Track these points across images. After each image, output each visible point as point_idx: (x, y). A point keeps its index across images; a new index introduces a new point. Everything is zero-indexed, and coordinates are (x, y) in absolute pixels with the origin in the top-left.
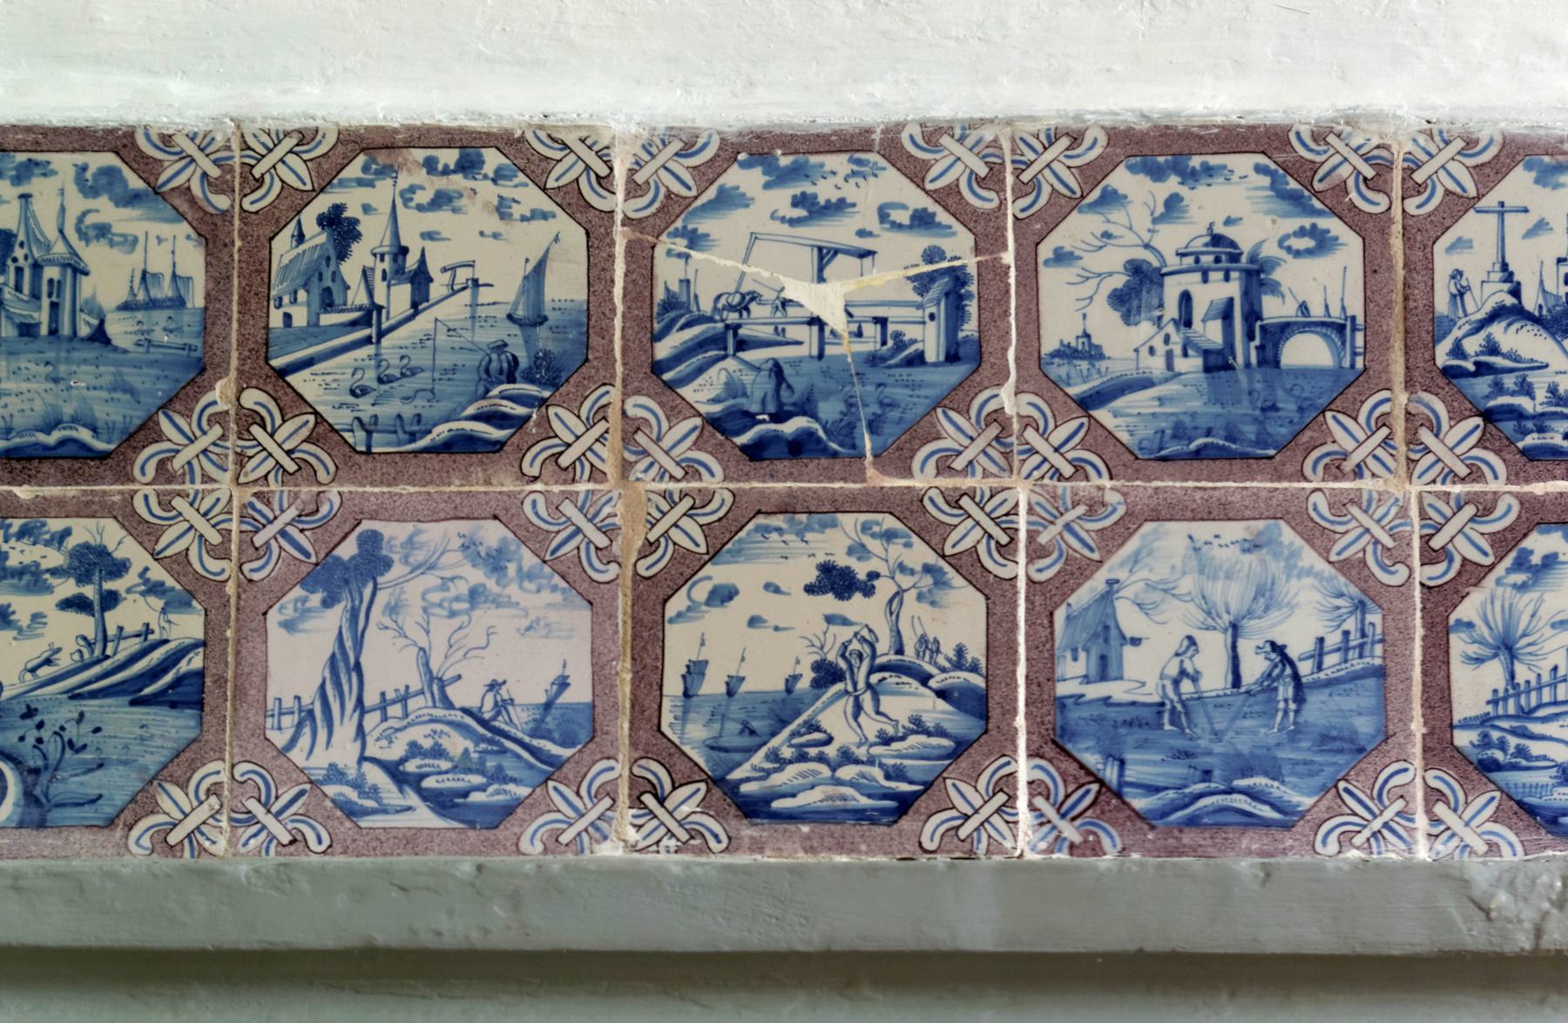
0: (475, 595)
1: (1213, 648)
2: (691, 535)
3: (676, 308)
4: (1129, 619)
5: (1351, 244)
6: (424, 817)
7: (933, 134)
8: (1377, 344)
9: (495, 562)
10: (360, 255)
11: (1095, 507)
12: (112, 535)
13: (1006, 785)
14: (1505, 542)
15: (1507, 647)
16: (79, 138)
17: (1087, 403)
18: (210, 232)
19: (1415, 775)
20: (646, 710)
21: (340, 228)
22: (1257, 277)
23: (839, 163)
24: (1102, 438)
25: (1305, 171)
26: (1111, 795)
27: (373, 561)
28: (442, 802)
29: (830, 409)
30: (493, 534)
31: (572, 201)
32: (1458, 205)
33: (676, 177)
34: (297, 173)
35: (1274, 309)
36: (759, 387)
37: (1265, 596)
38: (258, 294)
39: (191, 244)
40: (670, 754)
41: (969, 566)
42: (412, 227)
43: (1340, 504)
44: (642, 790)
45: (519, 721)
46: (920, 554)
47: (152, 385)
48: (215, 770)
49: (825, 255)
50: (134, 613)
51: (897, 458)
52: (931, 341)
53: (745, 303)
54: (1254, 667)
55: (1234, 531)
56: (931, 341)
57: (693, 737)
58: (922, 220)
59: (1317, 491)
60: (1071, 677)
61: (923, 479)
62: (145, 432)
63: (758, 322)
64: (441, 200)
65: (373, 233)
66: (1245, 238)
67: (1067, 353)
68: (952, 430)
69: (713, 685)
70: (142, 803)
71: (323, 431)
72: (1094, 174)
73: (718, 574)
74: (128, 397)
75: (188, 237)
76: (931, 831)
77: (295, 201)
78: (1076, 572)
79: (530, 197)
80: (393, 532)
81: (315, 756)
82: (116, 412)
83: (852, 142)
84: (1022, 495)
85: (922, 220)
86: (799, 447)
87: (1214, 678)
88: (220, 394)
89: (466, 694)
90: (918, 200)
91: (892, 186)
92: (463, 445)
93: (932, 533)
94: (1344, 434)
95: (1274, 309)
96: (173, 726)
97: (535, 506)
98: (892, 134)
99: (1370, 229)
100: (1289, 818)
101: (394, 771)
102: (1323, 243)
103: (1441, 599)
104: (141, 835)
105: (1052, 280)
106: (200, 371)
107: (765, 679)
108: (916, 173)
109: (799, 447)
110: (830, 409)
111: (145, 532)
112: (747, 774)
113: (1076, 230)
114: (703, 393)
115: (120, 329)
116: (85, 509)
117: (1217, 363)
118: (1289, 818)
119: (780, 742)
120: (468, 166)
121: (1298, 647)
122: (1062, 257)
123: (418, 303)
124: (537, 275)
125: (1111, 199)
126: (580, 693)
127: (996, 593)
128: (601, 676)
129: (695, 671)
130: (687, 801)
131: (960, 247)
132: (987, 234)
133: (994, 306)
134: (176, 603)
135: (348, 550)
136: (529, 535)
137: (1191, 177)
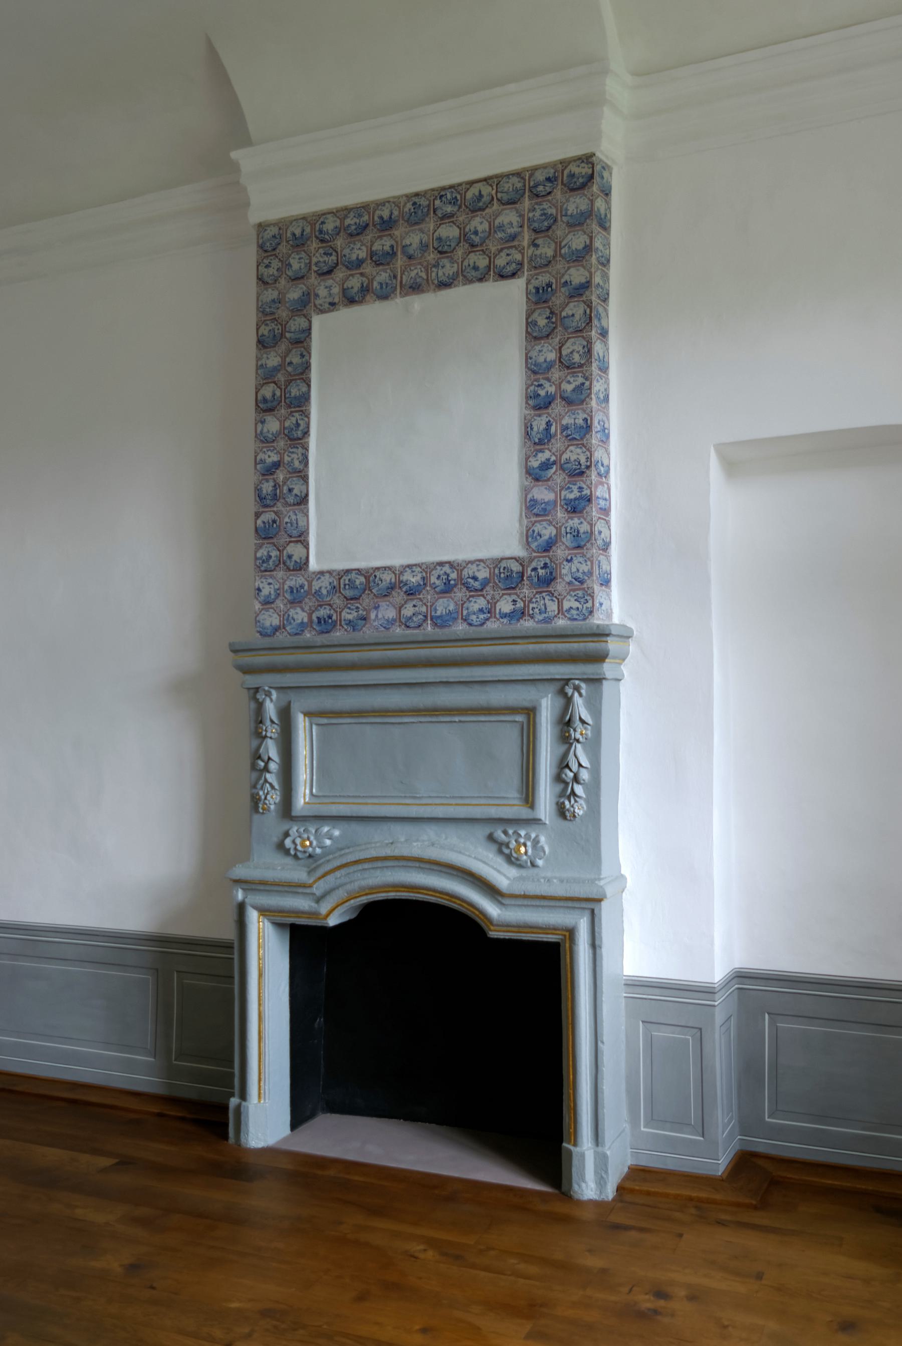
0: (387, 609)
1: (444, 610)
2: (403, 602)
3: (402, 582)
4: (437, 608)
5: (456, 572)
6: (383, 629)
7: (422, 564)
8: (458, 581)
9: (388, 606)
10: (377, 579)
11: (435, 598)
12: (358, 605)
13: (428, 624)
14: (468, 599)
15: (468, 609)
16: (355, 570)
17: (434, 588)
18: (365, 577)
19: (460, 621)
20: (400, 618)
21: (375, 576)
22: (448, 575)
23: (414, 567)
24: (435, 592)
25: (452, 565)
26: (436, 624)
27: (379, 606)
28: (384, 627)
29: (414, 590)
30: (388, 603)
31: (394, 572)
32: (465, 567)
33: (402, 569)
34: (372, 571)
35: (450, 578)
36: (408, 588)
37: (448, 605)
38: (369, 583)
39: (605, 1039)
40: (402, 622)
41: (425, 604)
42: (381, 575)
43: (455, 596)
44: (400, 626)
45: (390, 620)
46: (421, 603)
47: (361, 592)
48: (367, 626)
49: (414, 576)
50: (361, 612)
51: (419, 594)
52: (422, 583)
53: (407, 581)
54: (447, 612)
55: (446, 599)
56: (422, 583)
57: (403, 620)
58: (421, 572)
59: (453, 595)
60: (433, 614)
61: (421, 596)
62: (361, 596)
63: (408, 583)
64: (383, 573)
65: (378, 576)
66: (447, 572)
67: (433, 584)
68: (424, 591)
69: (405, 616)
70: (361, 629)
71: (375, 595)
72: (435, 567)
73: (405, 606)
74: (562, 360)
75: (603, 1042)
76: (422, 628)
77: (372, 574)
78: (433, 604)
79: (390, 572)
80: (380, 604)
81: (376, 623)
82: (359, 594)
83: (415, 565)
84: (429, 597)
85: (421, 572)
86: (412, 594)
87: (444, 613)
88: (367, 592)
89: (386, 618)
90: (421, 570)
91: (419, 569)
92: (386, 595)
93: (422, 601)
94: (455, 590)
95: (450, 578)
96: (363, 622)
97: (391, 601)
98: (419, 564)
99: (457, 570)
100: (450, 625)
101: (381, 625)
102: (454, 572)
103: (462, 605)
104: (362, 632)
105: (432, 577)
106: (365, 590)
107: (409, 615)
108: (421, 568)
109: (412, 594)
110: (414, 590)
111: (361, 605)
112: (408, 624)
113: (434, 572)
114: (404, 589)
115: (359, 587)
116: (357, 603)
117: (445, 584)
118: (450, 625)
119: (410, 621)
120: (385, 570)
121: (451, 609)
122: (433, 575)
123: (382, 582)
124: (391, 579)
125: (436, 569)
126: (395, 617)
127: (427, 606)
128: (397, 616)
129: (404, 615)
130: (403, 626)
131: (424, 574)
132: (426, 573)
133: (427, 581)
134: (364, 611)
135: (377, 605)
136: (391, 603)
137: (443, 566)
